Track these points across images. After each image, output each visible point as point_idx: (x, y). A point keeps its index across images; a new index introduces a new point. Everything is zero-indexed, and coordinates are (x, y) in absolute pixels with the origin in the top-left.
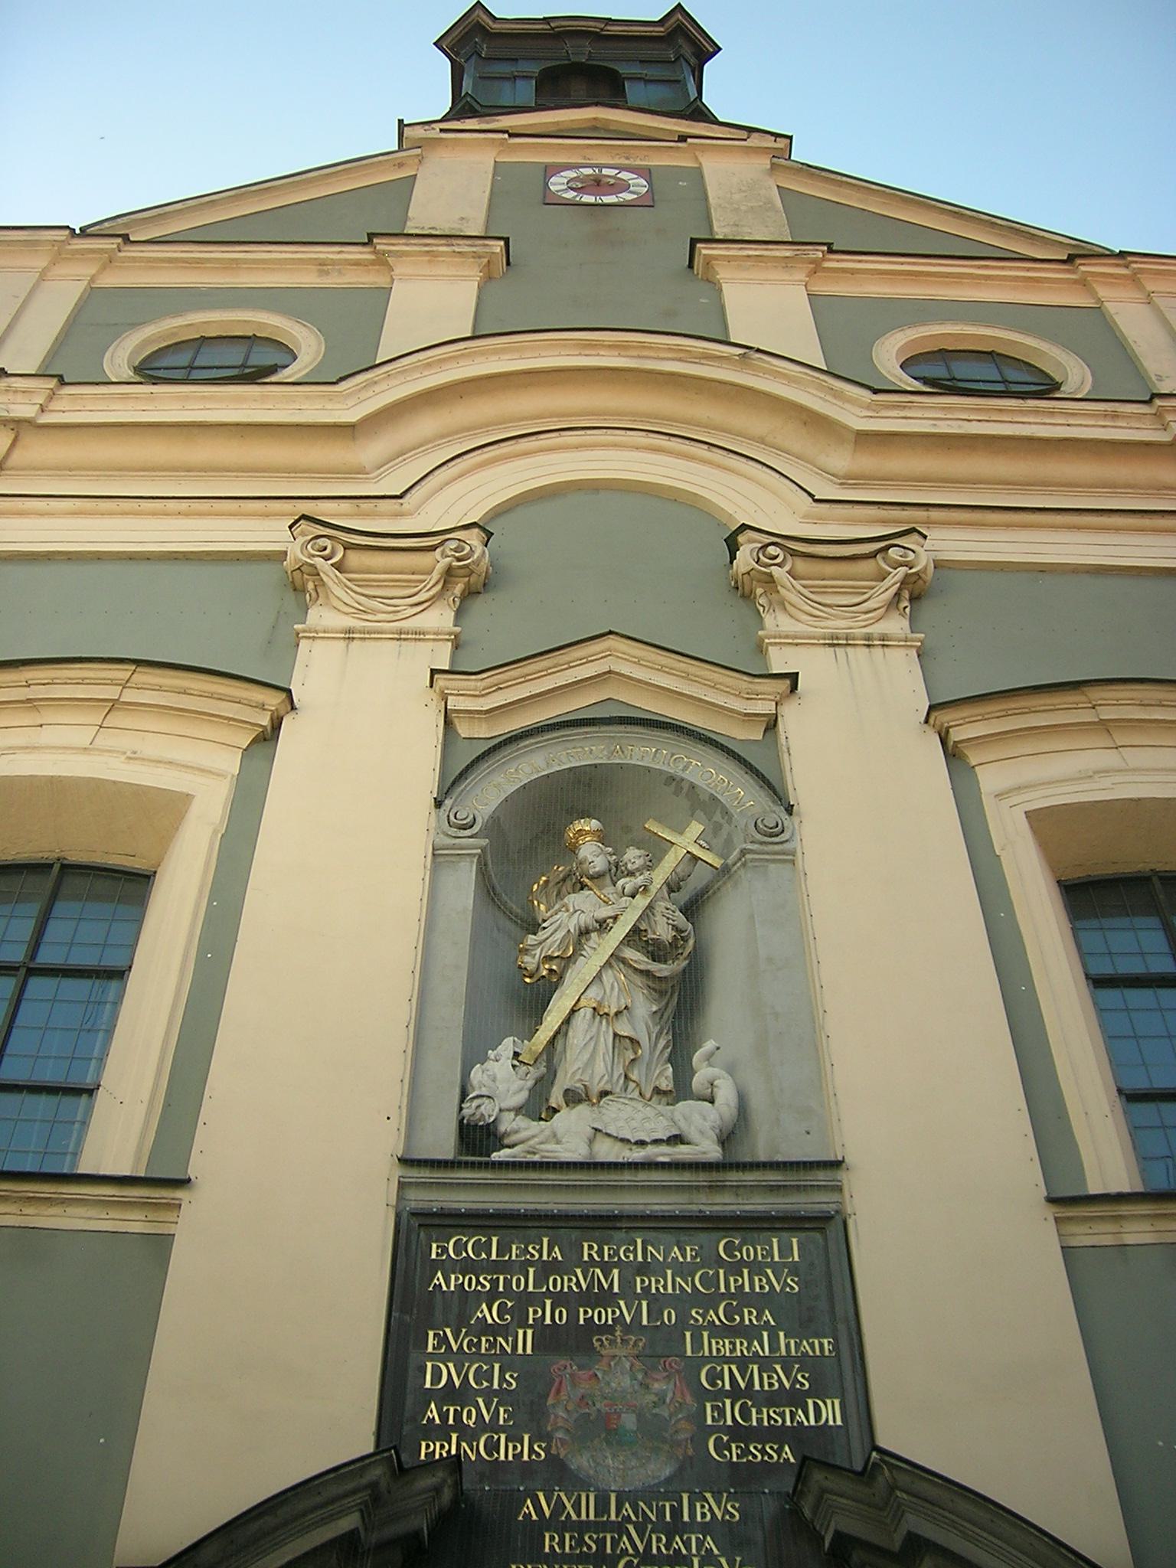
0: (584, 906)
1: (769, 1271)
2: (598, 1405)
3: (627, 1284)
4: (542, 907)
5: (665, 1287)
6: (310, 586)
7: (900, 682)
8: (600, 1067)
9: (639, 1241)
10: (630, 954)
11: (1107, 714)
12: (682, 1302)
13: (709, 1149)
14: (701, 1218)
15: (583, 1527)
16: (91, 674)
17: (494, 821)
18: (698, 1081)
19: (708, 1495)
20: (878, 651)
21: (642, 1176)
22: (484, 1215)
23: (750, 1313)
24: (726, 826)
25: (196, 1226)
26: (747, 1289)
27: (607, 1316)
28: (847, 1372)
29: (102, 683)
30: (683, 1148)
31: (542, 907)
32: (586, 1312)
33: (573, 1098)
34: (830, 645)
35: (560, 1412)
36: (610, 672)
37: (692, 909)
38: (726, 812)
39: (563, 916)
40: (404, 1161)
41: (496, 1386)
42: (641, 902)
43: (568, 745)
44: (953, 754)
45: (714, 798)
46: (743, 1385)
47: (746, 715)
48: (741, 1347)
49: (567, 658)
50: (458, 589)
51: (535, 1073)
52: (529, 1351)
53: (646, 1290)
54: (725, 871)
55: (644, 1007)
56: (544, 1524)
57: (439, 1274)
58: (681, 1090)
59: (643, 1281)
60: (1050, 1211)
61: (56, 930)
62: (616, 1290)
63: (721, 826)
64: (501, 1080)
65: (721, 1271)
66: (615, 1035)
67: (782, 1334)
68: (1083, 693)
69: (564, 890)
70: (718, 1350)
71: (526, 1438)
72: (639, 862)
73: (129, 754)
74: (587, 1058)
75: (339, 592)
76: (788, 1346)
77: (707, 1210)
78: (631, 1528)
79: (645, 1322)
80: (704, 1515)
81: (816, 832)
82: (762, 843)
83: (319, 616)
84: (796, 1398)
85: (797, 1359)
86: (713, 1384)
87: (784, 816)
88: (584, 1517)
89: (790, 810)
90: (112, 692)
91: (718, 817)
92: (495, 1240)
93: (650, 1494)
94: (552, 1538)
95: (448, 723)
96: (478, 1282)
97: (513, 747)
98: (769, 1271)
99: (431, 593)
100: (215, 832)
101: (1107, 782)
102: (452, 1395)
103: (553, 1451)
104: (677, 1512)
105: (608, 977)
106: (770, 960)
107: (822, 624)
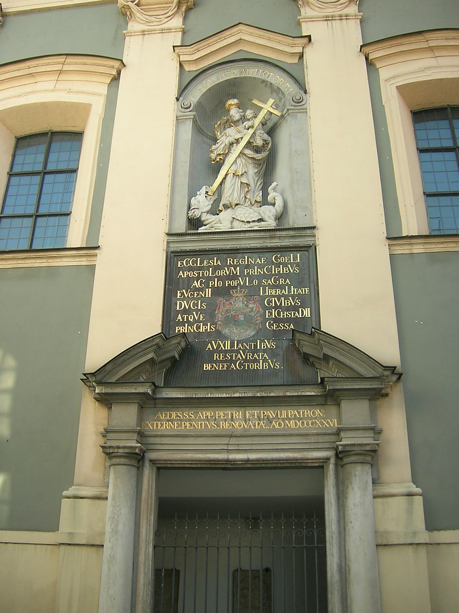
0: (232, 133)
1: (289, 266)
2: (232, 313)
3: (242, 272)
4: (219, 133)
5: (254, 272)
6: (128, 13)
7: (352, 33)
8: (235, 195)
9: (246, 257)
10: (248, 152)
11: (432, 44)
12: (260, 277)
13: (271, 223)
14: (267, 248)
15: (226, 352)
16: (51, 61)
17: (199, 103)
18: (270, 198)
19: (266, 341)
20: (344, 22)
21: (247, 234)
22: (196, 251)
23: (282, 280)
24: (283, 98)
25: (102, 261)
26: (281, 272)
27: (235, 283)
28: (313, 300)
29: (54, 64)
30: (262, 223)
31: (219, 133)
32: (228, 282)
33: (226, 207)
34: (325, 20)
35: (219, 316)
36: (240, 39)
37: (272, 132)
38: (283, 94)
39: (224, 137)
40: (168, 234)
41: (199, 308)
42: (251, 131)
43: (225, 71)
44: (370, 63)
45: (278, 88)
46: (279, 304)
47: (291, 53)
48: (278, 292)
49: (224, 35)
50: (184, 8)
51: (214, 198)
52: (210, 296)
53: (248, 274)
54: (282, 116)
55: (252, 170)
56: (214, 351)
57: (181, 272)
58: (264, 202)
59: (247, 271)
60: (387, 242)
61: (53, 157)
62: (238, 274)
63: (282, 98)
64: (202, 203)
65: (273, 266)
66: (241, 182)
67: (292, 287)
68: (423, 36)
69: (226, 126)
70: (271, 293)
71: (209, 324)
72: (251, 115)
73: (68, 90)
74: (232, 192)
75: (138, 15)
76: (294, 291)
77: (269, 245)
78: (241, 351)
79: (247, 285)
80: (264, 347)
81: (314, 101)
82: (295, 106)
83: (133, 26)
84: (295, 308)
85: (297, 295)
86: (269, 304)
87: (303, 94)
88: (226, 349)
89: (305, 92)
90: (59, 67)
91: (280, 95)
92: (199, 259)
93: (247, 341)
94: (217, 355)
95: (181, 65)
96: (194, 274)
97: (204, 74)
98: (289, 266)
99: (173, 12)
100: (100, 118)
101: (429, 72)
102: (186, 311)
103: (217, 328)
104: (256, 346)
105: (239, 161)
106: (296, 151)
107: (323, 11)
